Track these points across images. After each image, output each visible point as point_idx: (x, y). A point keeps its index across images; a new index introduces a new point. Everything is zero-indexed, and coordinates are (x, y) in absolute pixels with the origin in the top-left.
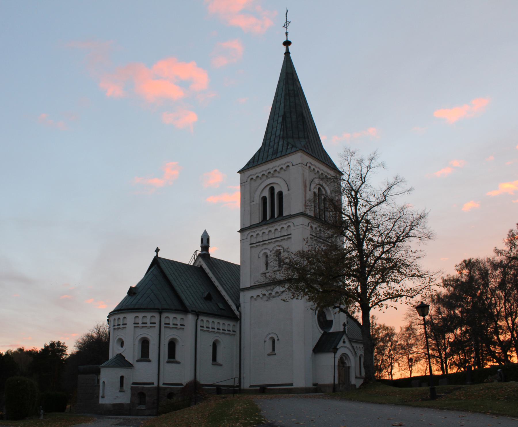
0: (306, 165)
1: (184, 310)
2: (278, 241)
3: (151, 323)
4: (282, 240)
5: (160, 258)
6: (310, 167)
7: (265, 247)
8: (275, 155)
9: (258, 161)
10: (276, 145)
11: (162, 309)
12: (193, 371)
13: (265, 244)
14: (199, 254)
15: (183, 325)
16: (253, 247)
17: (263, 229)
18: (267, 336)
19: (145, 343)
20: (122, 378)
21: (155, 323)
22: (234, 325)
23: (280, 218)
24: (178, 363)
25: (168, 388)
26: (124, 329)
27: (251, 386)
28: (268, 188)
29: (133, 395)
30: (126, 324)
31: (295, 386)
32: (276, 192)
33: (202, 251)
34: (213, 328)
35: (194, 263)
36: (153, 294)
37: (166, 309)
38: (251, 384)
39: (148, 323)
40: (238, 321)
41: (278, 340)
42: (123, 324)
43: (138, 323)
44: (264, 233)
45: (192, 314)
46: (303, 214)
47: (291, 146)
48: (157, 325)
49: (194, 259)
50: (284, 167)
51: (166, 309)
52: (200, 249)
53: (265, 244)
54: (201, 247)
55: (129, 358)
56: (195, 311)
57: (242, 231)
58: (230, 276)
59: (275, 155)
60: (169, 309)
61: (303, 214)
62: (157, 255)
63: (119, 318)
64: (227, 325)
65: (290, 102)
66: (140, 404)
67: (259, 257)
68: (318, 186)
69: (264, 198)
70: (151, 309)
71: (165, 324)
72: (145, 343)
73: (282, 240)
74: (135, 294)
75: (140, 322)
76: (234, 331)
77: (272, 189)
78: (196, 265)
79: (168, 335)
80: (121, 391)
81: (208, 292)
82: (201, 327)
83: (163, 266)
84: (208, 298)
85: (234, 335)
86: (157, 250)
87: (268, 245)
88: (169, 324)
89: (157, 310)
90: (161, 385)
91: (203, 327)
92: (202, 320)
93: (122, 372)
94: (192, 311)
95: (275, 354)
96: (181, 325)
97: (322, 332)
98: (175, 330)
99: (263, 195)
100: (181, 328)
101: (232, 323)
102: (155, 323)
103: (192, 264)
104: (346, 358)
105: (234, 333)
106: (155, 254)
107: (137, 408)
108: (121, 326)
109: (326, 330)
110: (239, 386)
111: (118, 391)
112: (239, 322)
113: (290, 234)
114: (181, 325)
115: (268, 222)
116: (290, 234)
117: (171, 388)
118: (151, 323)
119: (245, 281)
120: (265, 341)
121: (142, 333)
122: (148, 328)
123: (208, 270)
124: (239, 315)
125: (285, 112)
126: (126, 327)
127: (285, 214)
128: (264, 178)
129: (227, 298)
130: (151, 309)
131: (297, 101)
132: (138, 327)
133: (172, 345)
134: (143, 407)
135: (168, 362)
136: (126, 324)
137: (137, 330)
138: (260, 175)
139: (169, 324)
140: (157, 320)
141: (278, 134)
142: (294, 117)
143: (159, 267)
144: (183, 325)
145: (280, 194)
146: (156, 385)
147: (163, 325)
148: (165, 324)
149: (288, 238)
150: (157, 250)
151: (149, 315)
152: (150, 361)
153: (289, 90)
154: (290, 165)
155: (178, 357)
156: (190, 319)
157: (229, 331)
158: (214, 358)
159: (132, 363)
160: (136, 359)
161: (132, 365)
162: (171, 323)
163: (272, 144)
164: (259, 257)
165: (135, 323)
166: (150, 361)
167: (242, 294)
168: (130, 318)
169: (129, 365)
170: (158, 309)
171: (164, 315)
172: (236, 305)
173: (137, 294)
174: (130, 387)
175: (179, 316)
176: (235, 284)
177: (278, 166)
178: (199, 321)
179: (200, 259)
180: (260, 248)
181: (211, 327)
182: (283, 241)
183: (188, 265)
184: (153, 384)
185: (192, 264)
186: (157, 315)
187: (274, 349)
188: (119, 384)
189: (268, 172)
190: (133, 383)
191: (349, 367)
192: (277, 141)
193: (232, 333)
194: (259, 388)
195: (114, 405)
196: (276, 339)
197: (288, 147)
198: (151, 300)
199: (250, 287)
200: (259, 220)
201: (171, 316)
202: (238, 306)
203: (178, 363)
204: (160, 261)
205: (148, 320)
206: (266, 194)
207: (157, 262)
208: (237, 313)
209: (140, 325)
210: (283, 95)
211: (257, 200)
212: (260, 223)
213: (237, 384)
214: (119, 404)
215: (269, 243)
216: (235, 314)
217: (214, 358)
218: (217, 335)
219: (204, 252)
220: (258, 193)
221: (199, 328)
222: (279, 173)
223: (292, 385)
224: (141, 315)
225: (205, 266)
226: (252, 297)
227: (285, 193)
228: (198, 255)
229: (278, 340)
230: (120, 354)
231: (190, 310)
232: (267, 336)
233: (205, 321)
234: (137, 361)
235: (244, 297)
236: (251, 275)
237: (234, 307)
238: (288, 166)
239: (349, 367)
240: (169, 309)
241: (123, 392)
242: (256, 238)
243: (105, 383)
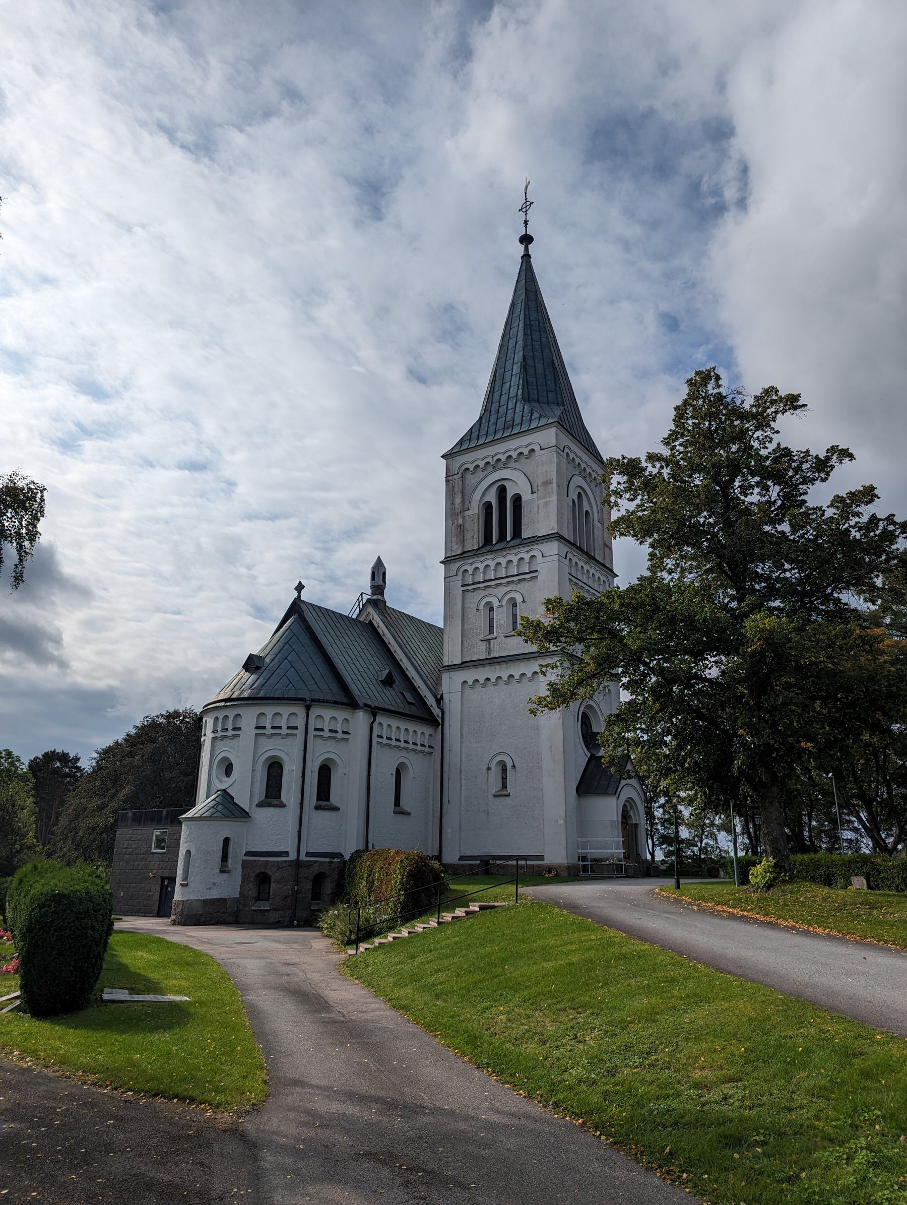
0: (563, 451)
1: (351, 703)
2: (512, 582)
3: (288, 728)
4: (520, 580)
5: (304, 602)
6: (567, 454)
7: (489, 591)
8: (510, 430)
9: (478, 439)
10: (510, 412)
11: (313, 700)
12: (299, 796)
13: (490, 586)
14: (368, 601)
15: (348, 733)
16: (468, 591)
17: (485, 560)
18: (492, 759)
19: (275, 769)
20: (226, 841)
21: (296, 728)
22: (430, 735)
23: (518, 541)
24: (336, 809)
25: (316, 862)
26: (236, 740)
27: (461, 858)
28: (494, 489)
29: (245, 878)
30: (240, 729)
31: (547, 862)
32: (509, 495)
33: (373, 594)
34: (388, 738)
35: (358, 616)
36: (292, 669)
37: (319, 701)
38: (462, 855)
39: (284, 727)
40: (438, 726)
41: (514, 766)
42: (234, 729)
43: (264, 728)
44: (488, 566)
45: (365, 711)
46: (558, 537)
47: (538, 416)
48: (300, 732)
49: (358, 609)
50: (526, 452)
51: (319, 701)
52: (369, 592)
53: (490, 586)
54: (372, 587)
55: (243, 800)
56: (370, 706)
57: (447, 561)
58: (419, 643)
59: (510, 430)
60: (323, 701)
61: (558, 537)
62: (299, 596)
63: (226, 717)
64: (419, 732)
65: (532, 340)
66: (258, 899)
67: (478, 610)
68: (579, 490)
69: (488, 506)
70: (290, 699)
71: (316, 729)
72: (275, 769)
73: (520, 580)
74: (258, 668)
75: (269, 726)
76: (430, 747)
77: (502, 491)
78: (362, 619)
79: (320, 752)
80: (223, 870)
81: (387, 671)
82: (378, 736)
83: (308, 616)
84: (388, 682)
85: (431, 753)
86: (300, 588)
87: (494, 588)
88: (322, 730)
89: (301, 702)
90: (303, 857)
91: (381, 737)
92: (380, 724)
93: (227, 829)
94: (366, 705)
95: (509, 795)
96: (343, 732)
97: (589, 755)
98: (332, 742)
99: (486, 499)
100: (343, 739)
101: (427, 730)
102: (296, 728)
103: (354, 617)
104: (631, 807)
105: (431, 750)
106: (296, 594)
107: (253, 908)
108: (230, 733)
109: (594, 752)
110: (439, 858)
111: (218, 871)
112: (440, 727)
113: (537, 571)
114: (343, 732)
115: (496, 547)
116: (537, 571)
117: (320, 862)
118: (288, 728)
119: (452, 653)
120: (489, 769)
121: (271, 748)
122: (283, 738)
123: (382, 629)
124: (440, 716)
125: (524, 357)
126: (239, 735)
127: (525, 534)
128: (490, 469)
129: (418, 682)
130: (290, 699)
131: (543, 339)
132: (264, 734)
133: (325, 772)
134: (264, 906)
135: (317, 808)
136: (240, 729)
137: (262, 740)
138: (482, 464)
139: (322, 730)
140: (300, 722)
141: (513, 393)
142: (539, 366)
143: (302, 619)
144: (348, 733)
145: (517, 499)
146: (292, 856)
147: (311, 733)
148: (316, 729)
149: (532, 578)
150: (300, 588)
151: (285, 710)
152: (283, 806)
153: (530, 320)
154: (537, 448)
155: (334, 799)
156: (361, 718)
157: (422, 745)
158: (397, 802)
159: (247, 810)
160: (256, 801)
161: (247, 813)
162: (326, 729)
163: (502, 410)
164: (478, 610)
165: (257, 728)
166: (283, 806)
167: (445, 677)
168: (249, 717)
169: (244, 815)
170: (304, 700)
171: (315, 711)
172: (435, 696)
173: (261, 670)
174: (241, 862)
175: (341, 714)
176: (428, 658)
177: (515, 450)
178: (375, 725)
179: (370, 609)
180: (503, 590)
181: (340, 731)
182: (523, 583)
183: (347, 617)
184: (286, 854)
185: (354, 617)
186: (300, 711)
187: (504, 786)
188: (220, 855)
189: (495, 459)
190: (249, 854)
191: (636, 825)
192: (511, 405)
193: (427, 749)
194: (478, 862)
195: (206, 902)
196: (509, 765)
197: (533, 418)
198: (291, 683)
199: (461, 664)
200: (478, 543)
201: (327, 713)
202: (439, 700)
203: (336, 809)
204: (302, 606)
205: (283, 723)
206: (492, 497)
207: (296, 609)
208: (436, 711)
209: (269, 731)
210: (520, 327)
211: (475, 509)
212: (480, 548)
213: (432, 851)
214: (219, 900)
215: (497, 585)
216: (431, 714)
217: (397, 802)
218: (404, 753)
219: (375, 597)
220: (477, 496)
221: (375, 739)
222: (515, 461)
223: (541, 858)
224: (269, 711)
225: (377, 620)
226: (465, 682)
227: (526, 496)
228: (364, 601)
229: (514, 766)
230: (224, 790)
231: (361, 705)
232: (492, 759)
233: (388, 725)
234: (260, 805)
235: (451, 684)
236: (462, 642)
237: (431, 701)
238: (533, 450)
239: (636, 825)
240: (323, 701)
241: (228, 872)
242: (473, 575)
243: (192, 853)
